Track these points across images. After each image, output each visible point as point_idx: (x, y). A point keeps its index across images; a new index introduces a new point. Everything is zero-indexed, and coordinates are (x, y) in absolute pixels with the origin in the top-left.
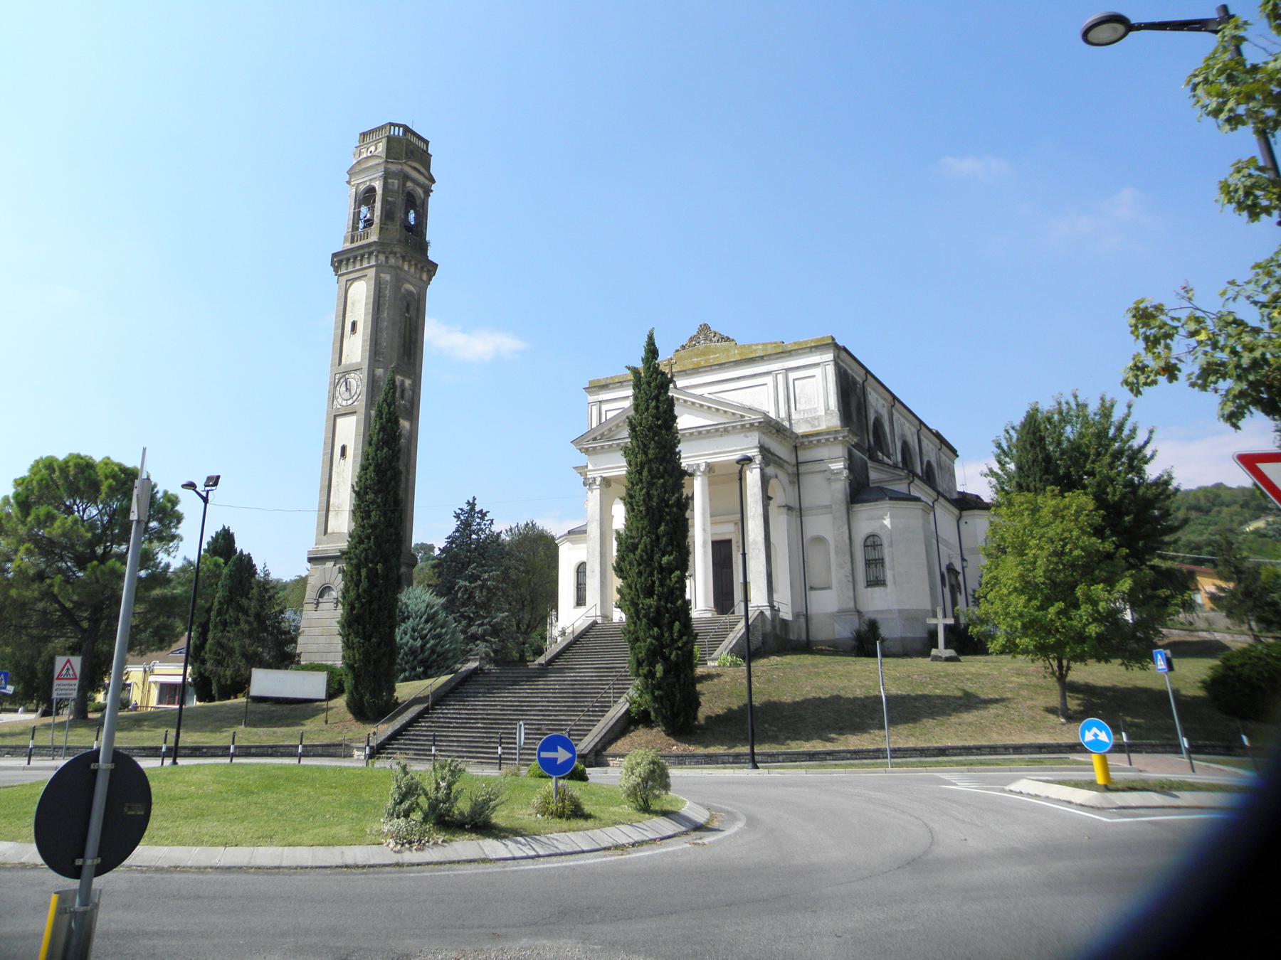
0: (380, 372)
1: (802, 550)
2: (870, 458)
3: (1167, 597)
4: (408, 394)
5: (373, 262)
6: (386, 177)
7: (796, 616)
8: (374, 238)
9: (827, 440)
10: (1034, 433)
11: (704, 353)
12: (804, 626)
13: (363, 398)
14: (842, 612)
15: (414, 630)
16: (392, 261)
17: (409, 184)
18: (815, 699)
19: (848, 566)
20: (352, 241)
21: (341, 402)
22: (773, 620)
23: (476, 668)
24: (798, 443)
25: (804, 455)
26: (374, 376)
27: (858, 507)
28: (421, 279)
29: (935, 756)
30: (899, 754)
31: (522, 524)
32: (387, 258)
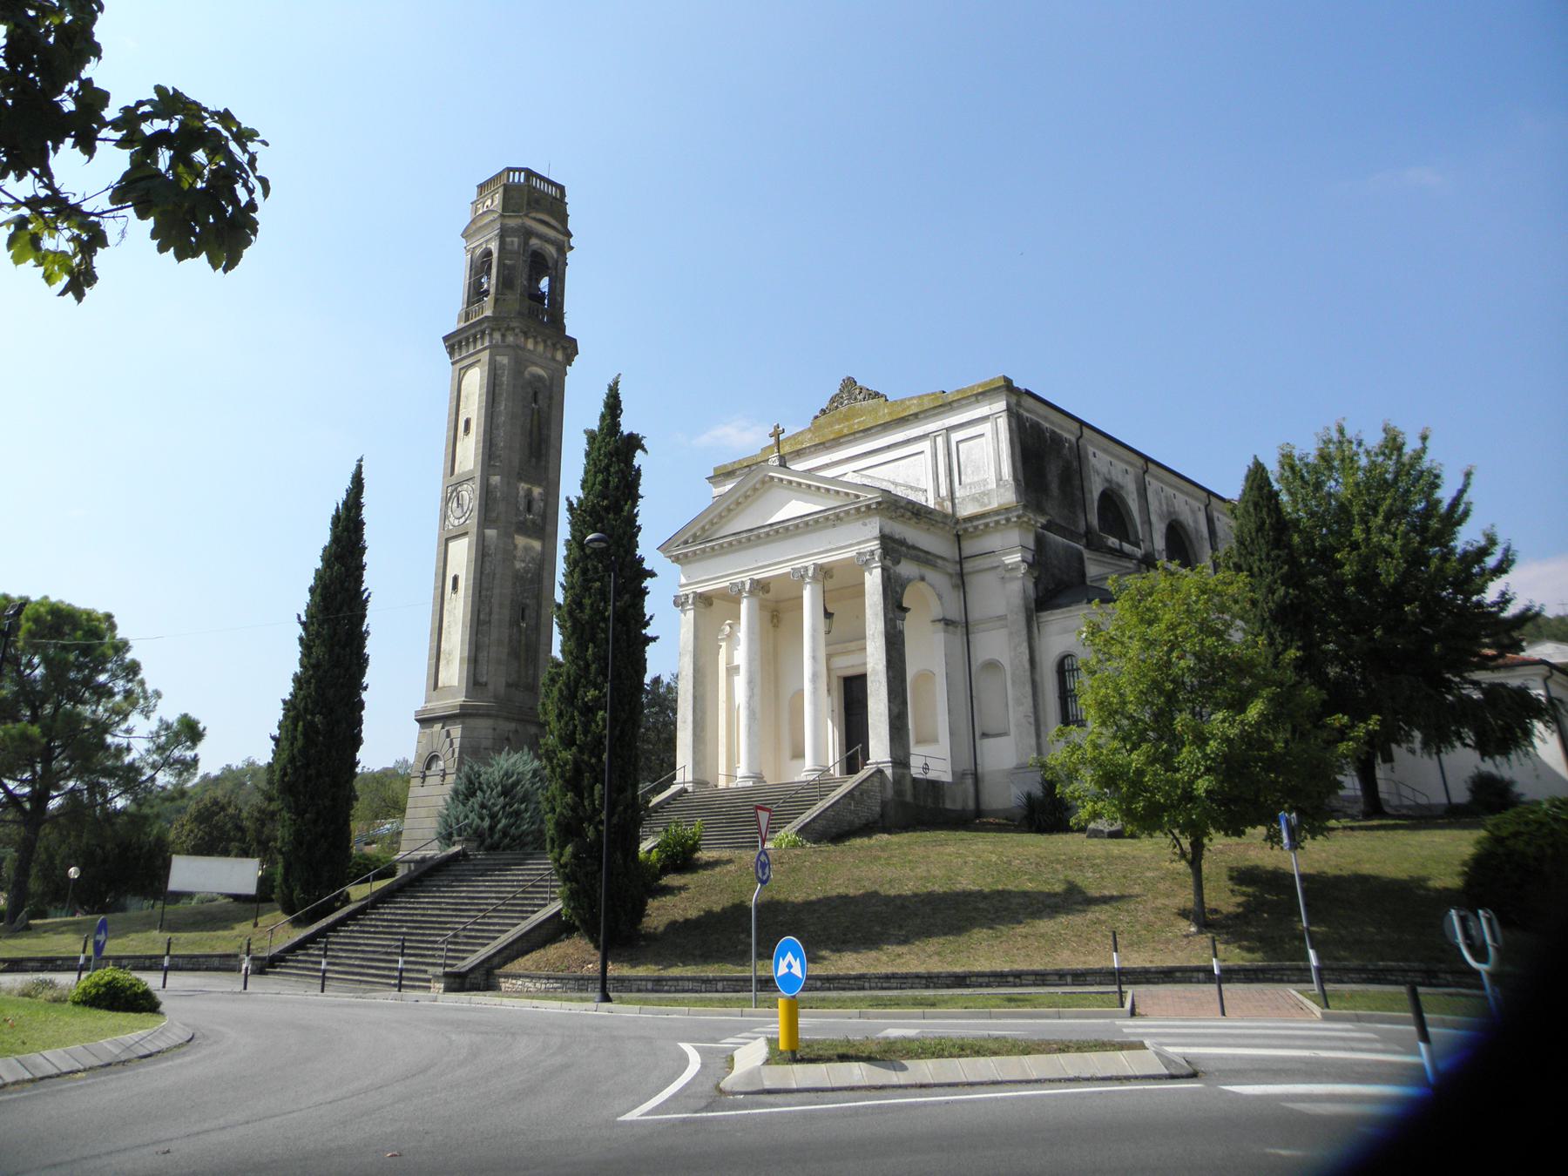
0: (496, 480)
1: (969, 679)
2: (1088, 546)
3: (1345, 726)
4: (538, 506)
5: (487, 344)
6: (502, 236)
7: (959, 776)
8: (488, 313)
9: (997, 522)
10: (1260, 488)
11: (846, 418)
12: (971, 790)
13: (475, 514)
14: (1021, 768)
15: (483, 806)
16: (510, 339)
17: (534, 242)
18: (840, 897)
19: (1029, 701)
20: (467, 319)
21: (453, 521)
22: (898, 780)
23: (457, 853)
24: (959, 529)
25: (970, 547)
26: (488, 485)
27: (1046, 616)
28: (553, 359)
29: (948, 987)
30: (894, 983)
31: (121, 633)
32: (503, 336)
